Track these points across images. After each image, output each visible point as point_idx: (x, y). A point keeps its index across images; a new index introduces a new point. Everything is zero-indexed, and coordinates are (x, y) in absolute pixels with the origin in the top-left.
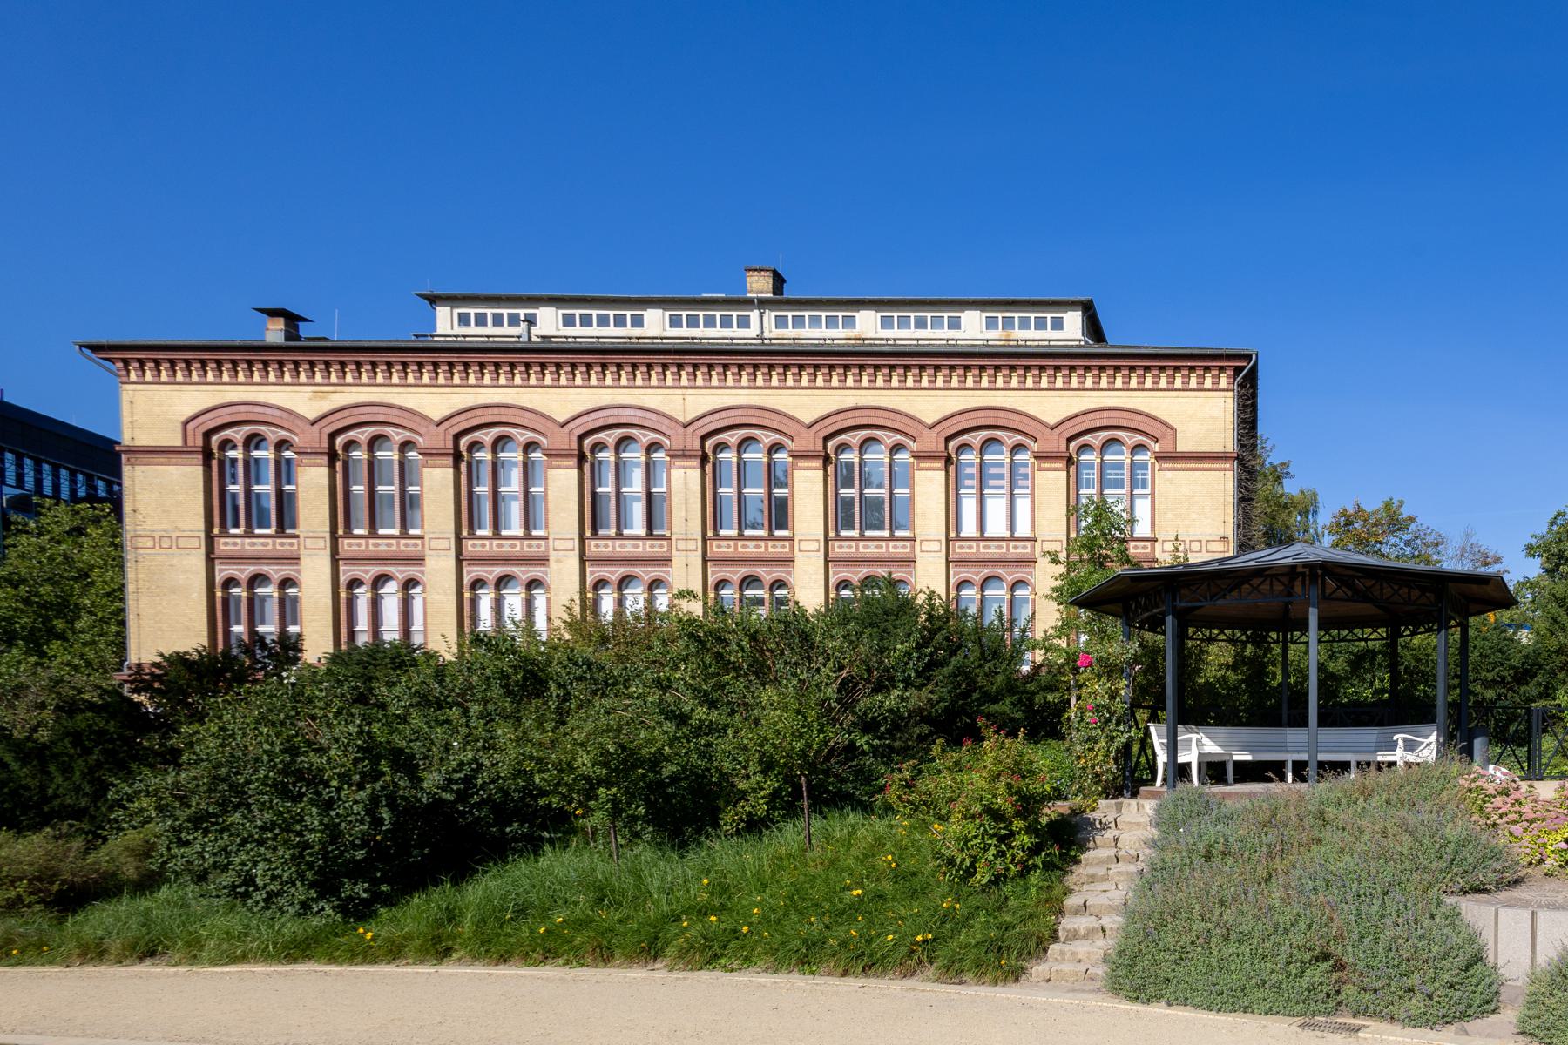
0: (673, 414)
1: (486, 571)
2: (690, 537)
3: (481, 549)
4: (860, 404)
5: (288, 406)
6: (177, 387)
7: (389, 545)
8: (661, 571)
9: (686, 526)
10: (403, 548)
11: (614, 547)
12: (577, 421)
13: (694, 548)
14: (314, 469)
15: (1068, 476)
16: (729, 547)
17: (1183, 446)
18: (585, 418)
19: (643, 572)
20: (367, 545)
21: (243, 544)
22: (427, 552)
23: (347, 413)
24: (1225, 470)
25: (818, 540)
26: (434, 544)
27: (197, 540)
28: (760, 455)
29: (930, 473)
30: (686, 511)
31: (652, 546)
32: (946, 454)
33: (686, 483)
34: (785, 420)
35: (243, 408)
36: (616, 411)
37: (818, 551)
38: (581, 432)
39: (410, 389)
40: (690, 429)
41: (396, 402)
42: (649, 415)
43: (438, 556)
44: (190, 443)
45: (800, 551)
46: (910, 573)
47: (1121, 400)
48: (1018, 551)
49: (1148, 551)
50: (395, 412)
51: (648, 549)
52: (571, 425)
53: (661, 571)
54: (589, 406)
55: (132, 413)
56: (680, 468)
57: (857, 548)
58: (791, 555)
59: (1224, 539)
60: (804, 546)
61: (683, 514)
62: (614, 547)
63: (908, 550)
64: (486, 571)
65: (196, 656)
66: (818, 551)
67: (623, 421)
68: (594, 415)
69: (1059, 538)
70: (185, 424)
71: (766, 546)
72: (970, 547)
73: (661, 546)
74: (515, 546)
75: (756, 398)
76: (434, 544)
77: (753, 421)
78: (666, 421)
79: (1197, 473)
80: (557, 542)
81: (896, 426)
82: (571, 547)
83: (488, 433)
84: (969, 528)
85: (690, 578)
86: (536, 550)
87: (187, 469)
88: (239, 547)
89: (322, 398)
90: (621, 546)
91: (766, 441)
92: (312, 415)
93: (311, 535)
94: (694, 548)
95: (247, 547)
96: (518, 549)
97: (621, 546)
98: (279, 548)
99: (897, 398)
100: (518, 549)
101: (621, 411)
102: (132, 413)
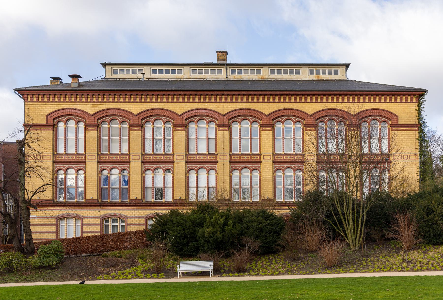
0: (219, 112)
1: (151, 167)
2: (225, 154)
3: (149, 159)
4: (285, 108)
5: (216, 110)
6: (45, 103)
7: (116, 158)
8: (213, 166)
9: (223, 150)
10: (121, 159)
11: (196, 158)
12: (185, 114)
13: (226, 158)
14: (92, 131)
15: (97, 132)
16: (237, 158)
17: (401, 122)
18: (188, 113)
19: (207, 167)
20: (109, 158)
21: (65, 158)
22: (131, 160)
23: (104, 112)
24: (416, 130)
25: (270, 155)
26: (134, 157)
27: (50, 156)
28: (118, 125)
29: (267, 132)
30: (224, 145)
31: (210, 158)
32: (53, 125)
33: (224, 136)
34: (259, 114)
35: (67, 111)
36: (199, 111)
37: (270, 159)
38: (98, 118)
39: (126, 103)
40: (225, 117)
41: (127, 109)
42: (210, 112)
43: (135, 161)
44: (49, 123)
45: (264, 159)
46: (259, 167)
47: (378, 106)
48: (255, 159)
49: (171, 159)
50: (121, 111)
51: (209, 159)
52: (183, 116)
53: (213, 166)
54: (190, 109)
55: (28, 112)
56: (221, 130)
57: (283, 158)
58: (85, 160)
59: (416, 154)
60: (265, 157)
61: (222, 146)
62: (196, 158)
63: (258, 159)
64: (151, 167)
65: (417, 193)
66: (270, 159)
67: (201, 114)
68: (191, 112)
69: (95, 154)
70: (47, 116)
71: (251, 157)
72: (106, 158)
73: (213, 157)
74: (161, 158)
75: (249, 106)
76: (134, 157)
77: (247, 114)
78: (217, 114)
79: (406, 131)
80: (177, 156)
81: (298, 115)
82: (182, 158)
83: (152, 118)
84: (61, 150)
85: (225, 169)
86: (169, 159)
87: (48, 132)
88: (63, 159)
89: (95, 107)
90: (199, 157)
91: (64, 120)
92: (92, 113)
93: (91, 154)
94: (226, 158)
95: (66, 159)
96: (162, 159)
97: (199, 157)
98: (77, 159)
99: (299, 106)
100: (162, 159)
101: (201, 111)
102: (28, 112)
